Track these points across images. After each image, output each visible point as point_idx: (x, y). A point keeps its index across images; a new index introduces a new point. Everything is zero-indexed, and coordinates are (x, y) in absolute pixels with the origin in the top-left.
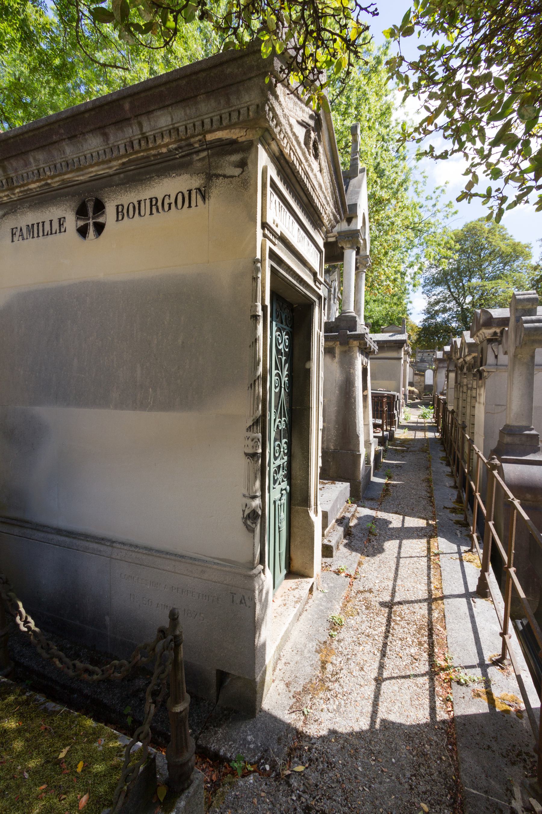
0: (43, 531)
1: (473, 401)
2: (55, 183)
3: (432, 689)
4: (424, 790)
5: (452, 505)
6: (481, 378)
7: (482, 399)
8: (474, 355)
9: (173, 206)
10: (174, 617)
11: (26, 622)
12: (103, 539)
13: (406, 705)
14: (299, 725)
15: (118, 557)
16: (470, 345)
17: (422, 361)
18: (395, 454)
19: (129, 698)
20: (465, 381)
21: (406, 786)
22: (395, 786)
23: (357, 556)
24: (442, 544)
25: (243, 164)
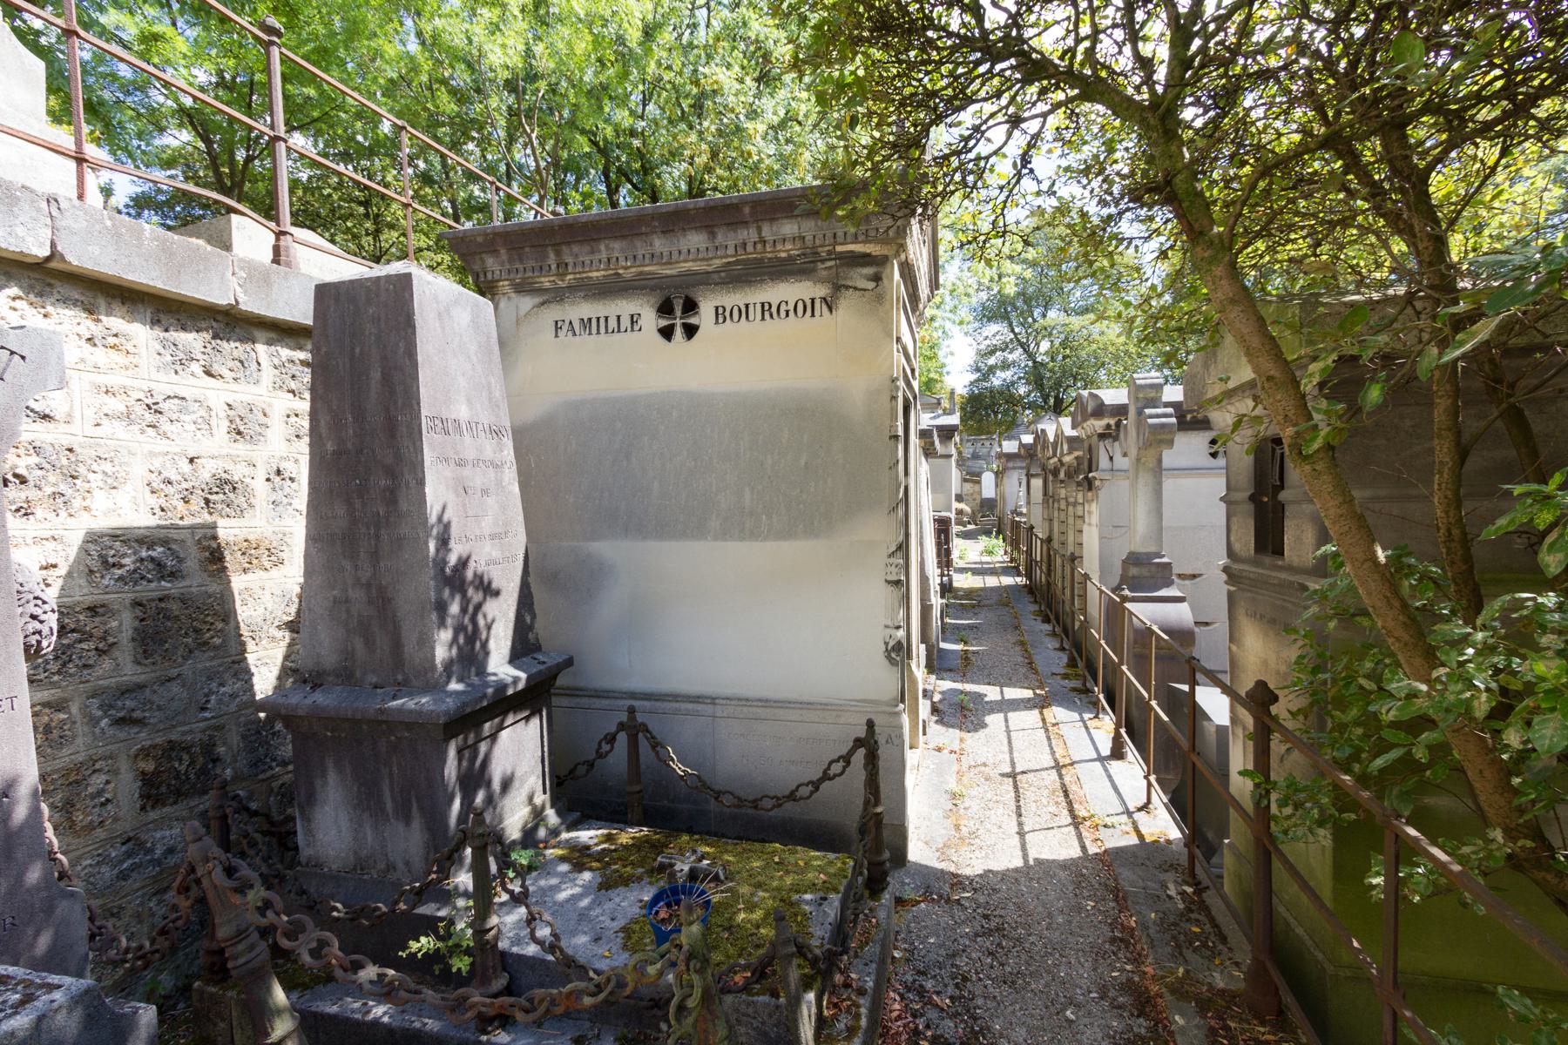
1: (1079, 522)
2: (628, 274)
5: (1063, 671)
6: (1090, 489)
7: (1095, 519)
8: (1077, 454)
9: (791, 313)
10: (870, 724)
13: (1058, 846)
14: (952, 869)
16: (1071, 440)
17: (975, 456)
18: (962, 610)
20: (1063, 493)
23: (955, 733)
24: (1057, 713)
25: (877, 278)
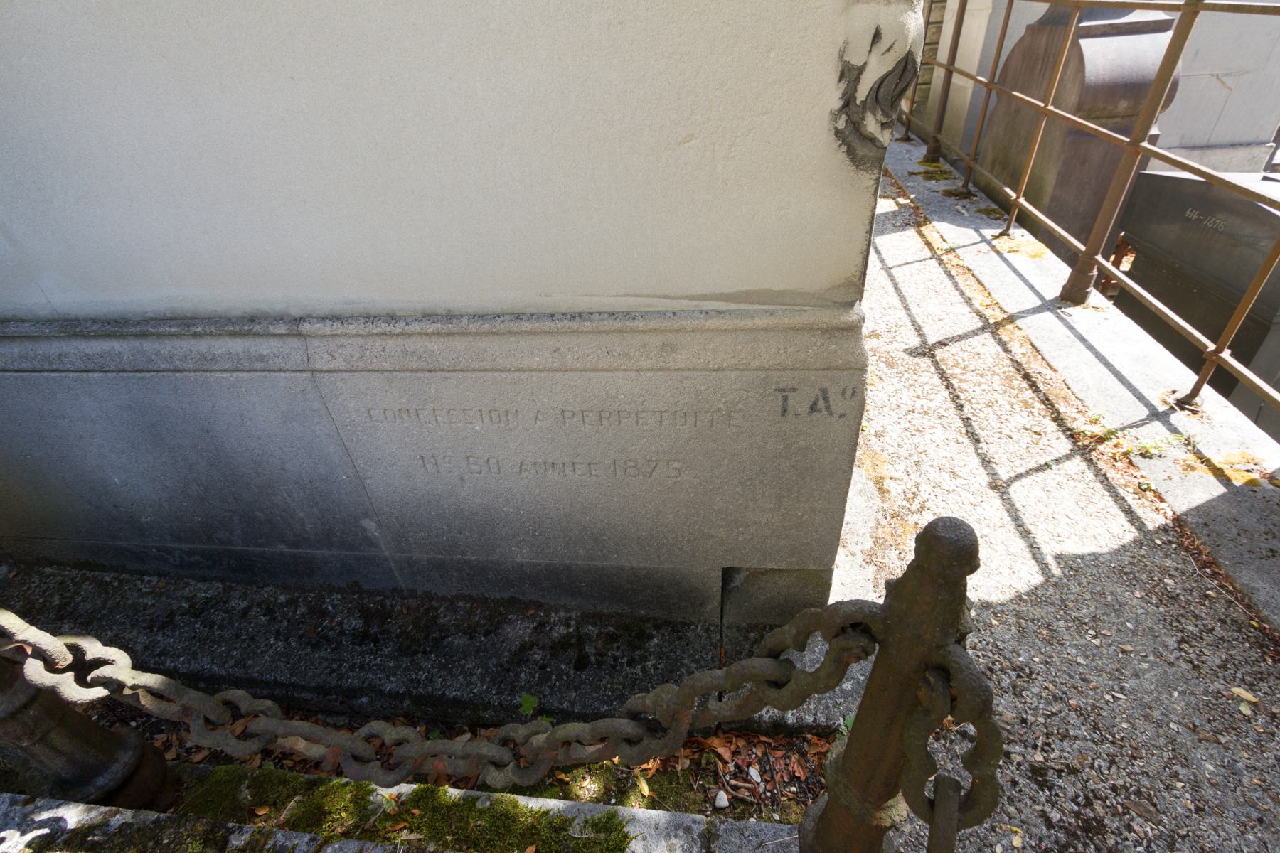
0: (12, 338)
3: (1100, 477)
4: (1218, 662)
5: (921, 169)
11: (82, 668)
12: (252, 319)
15: (339, 363)
19: (508, 670)
21: (1184, 666)
22: (1166, 672)
24: (944, 232)
